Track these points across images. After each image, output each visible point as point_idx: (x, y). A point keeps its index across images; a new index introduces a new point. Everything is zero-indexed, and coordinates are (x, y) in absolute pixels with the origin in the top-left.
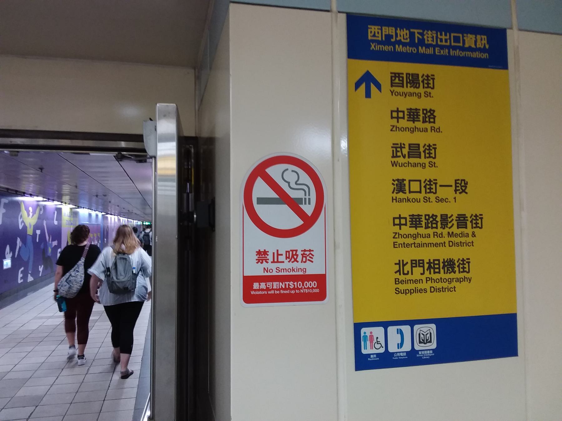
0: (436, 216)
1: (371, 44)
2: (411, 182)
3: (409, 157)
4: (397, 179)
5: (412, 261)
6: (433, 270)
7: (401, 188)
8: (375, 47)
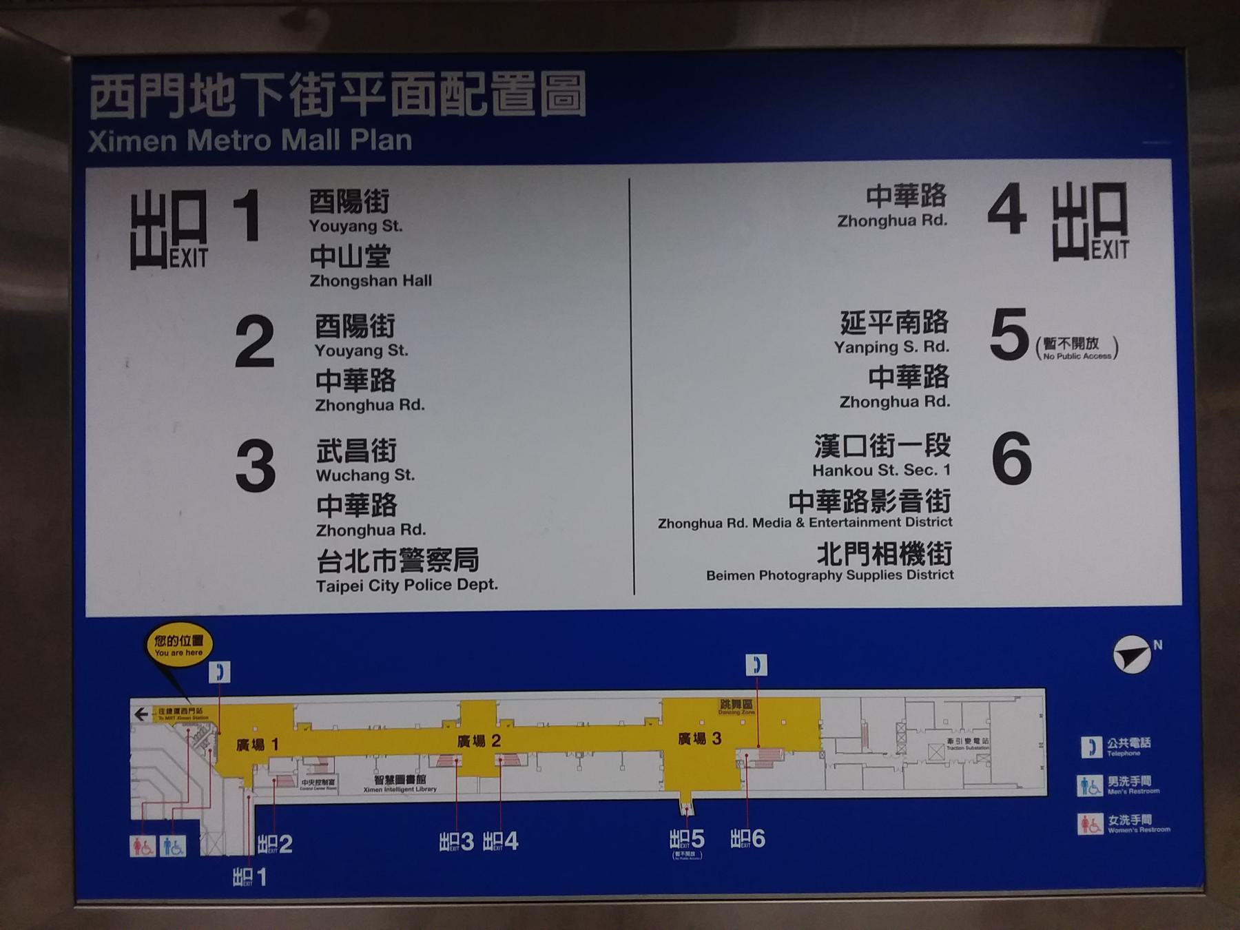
0: (865, 493)
1: (93, 133)
2: (862, 439)
3: (347, 461)
4: (823, 434)
5: (847, 544)
6: (883, 558)
7: (830, 449)
8: (105, 141)
